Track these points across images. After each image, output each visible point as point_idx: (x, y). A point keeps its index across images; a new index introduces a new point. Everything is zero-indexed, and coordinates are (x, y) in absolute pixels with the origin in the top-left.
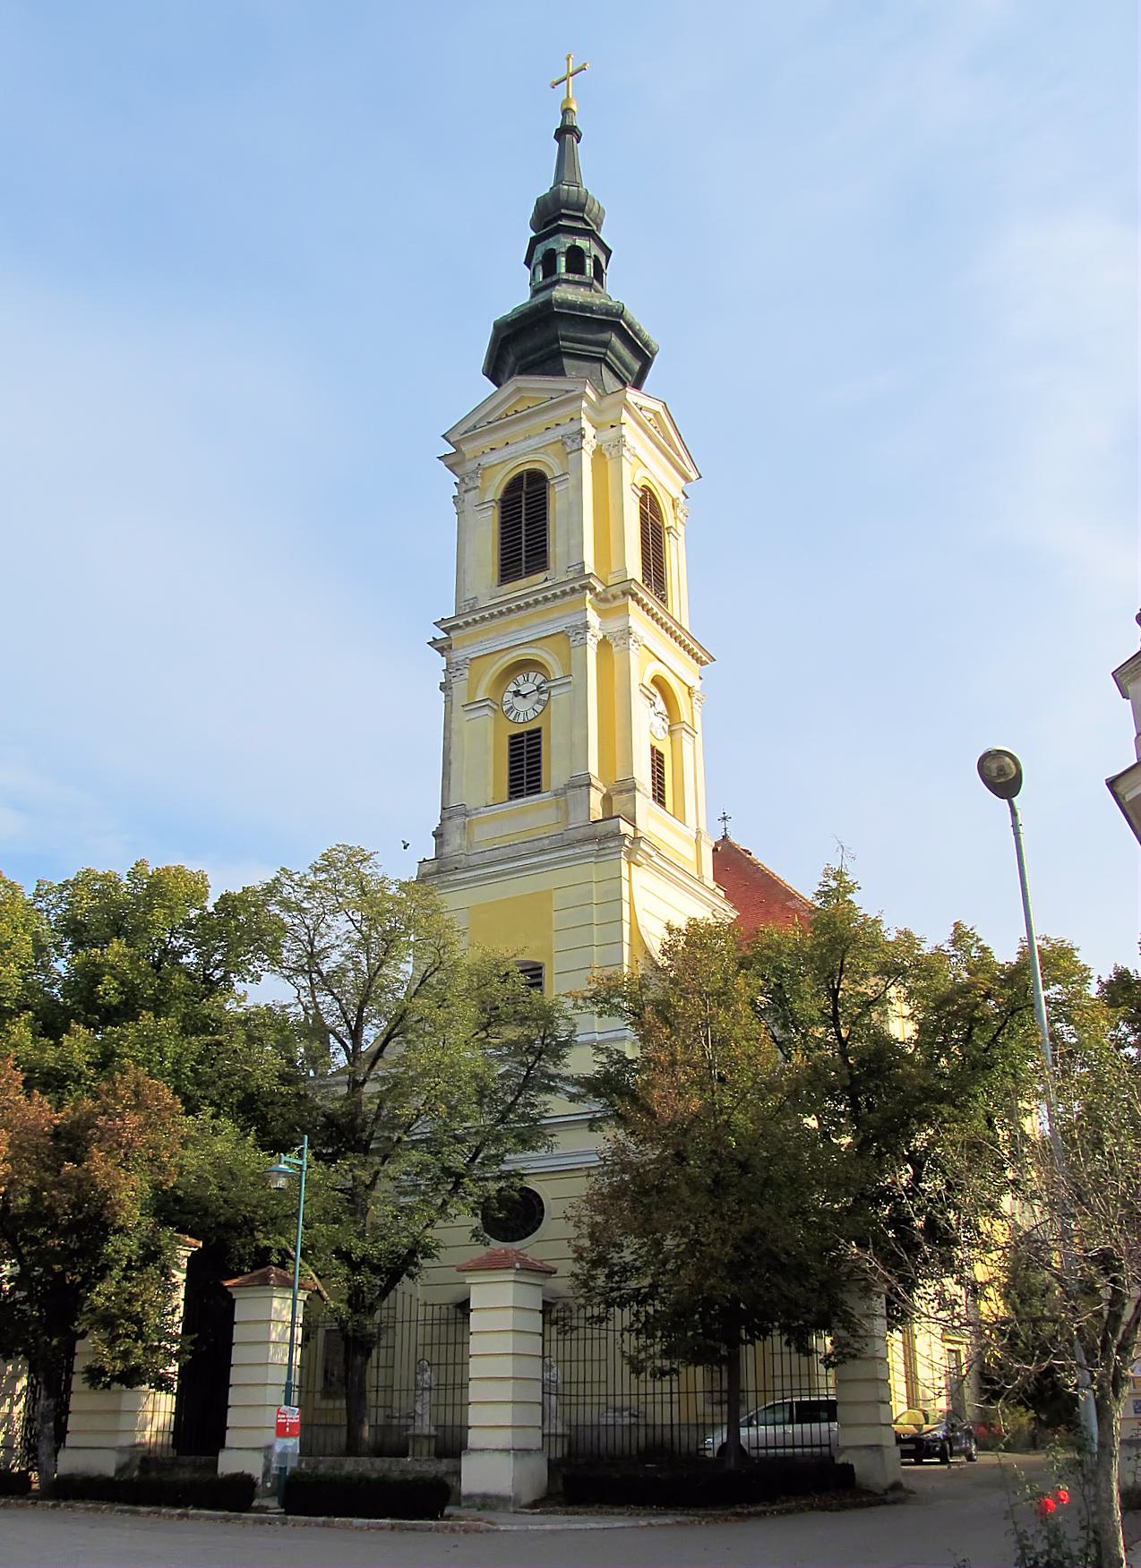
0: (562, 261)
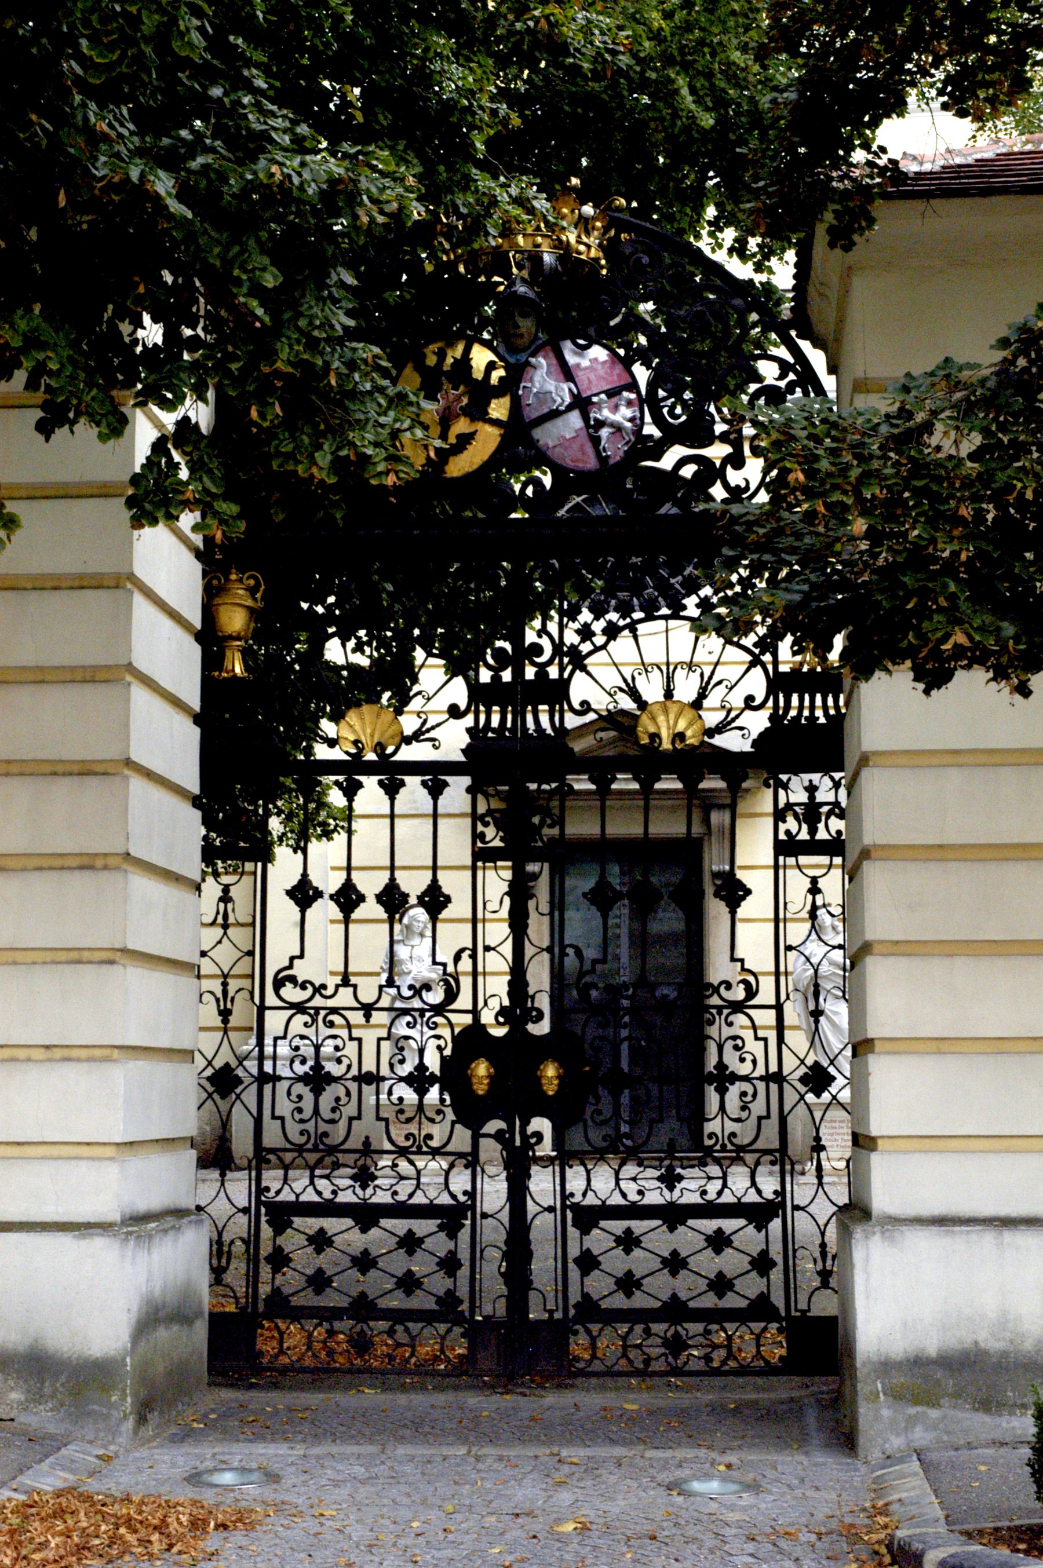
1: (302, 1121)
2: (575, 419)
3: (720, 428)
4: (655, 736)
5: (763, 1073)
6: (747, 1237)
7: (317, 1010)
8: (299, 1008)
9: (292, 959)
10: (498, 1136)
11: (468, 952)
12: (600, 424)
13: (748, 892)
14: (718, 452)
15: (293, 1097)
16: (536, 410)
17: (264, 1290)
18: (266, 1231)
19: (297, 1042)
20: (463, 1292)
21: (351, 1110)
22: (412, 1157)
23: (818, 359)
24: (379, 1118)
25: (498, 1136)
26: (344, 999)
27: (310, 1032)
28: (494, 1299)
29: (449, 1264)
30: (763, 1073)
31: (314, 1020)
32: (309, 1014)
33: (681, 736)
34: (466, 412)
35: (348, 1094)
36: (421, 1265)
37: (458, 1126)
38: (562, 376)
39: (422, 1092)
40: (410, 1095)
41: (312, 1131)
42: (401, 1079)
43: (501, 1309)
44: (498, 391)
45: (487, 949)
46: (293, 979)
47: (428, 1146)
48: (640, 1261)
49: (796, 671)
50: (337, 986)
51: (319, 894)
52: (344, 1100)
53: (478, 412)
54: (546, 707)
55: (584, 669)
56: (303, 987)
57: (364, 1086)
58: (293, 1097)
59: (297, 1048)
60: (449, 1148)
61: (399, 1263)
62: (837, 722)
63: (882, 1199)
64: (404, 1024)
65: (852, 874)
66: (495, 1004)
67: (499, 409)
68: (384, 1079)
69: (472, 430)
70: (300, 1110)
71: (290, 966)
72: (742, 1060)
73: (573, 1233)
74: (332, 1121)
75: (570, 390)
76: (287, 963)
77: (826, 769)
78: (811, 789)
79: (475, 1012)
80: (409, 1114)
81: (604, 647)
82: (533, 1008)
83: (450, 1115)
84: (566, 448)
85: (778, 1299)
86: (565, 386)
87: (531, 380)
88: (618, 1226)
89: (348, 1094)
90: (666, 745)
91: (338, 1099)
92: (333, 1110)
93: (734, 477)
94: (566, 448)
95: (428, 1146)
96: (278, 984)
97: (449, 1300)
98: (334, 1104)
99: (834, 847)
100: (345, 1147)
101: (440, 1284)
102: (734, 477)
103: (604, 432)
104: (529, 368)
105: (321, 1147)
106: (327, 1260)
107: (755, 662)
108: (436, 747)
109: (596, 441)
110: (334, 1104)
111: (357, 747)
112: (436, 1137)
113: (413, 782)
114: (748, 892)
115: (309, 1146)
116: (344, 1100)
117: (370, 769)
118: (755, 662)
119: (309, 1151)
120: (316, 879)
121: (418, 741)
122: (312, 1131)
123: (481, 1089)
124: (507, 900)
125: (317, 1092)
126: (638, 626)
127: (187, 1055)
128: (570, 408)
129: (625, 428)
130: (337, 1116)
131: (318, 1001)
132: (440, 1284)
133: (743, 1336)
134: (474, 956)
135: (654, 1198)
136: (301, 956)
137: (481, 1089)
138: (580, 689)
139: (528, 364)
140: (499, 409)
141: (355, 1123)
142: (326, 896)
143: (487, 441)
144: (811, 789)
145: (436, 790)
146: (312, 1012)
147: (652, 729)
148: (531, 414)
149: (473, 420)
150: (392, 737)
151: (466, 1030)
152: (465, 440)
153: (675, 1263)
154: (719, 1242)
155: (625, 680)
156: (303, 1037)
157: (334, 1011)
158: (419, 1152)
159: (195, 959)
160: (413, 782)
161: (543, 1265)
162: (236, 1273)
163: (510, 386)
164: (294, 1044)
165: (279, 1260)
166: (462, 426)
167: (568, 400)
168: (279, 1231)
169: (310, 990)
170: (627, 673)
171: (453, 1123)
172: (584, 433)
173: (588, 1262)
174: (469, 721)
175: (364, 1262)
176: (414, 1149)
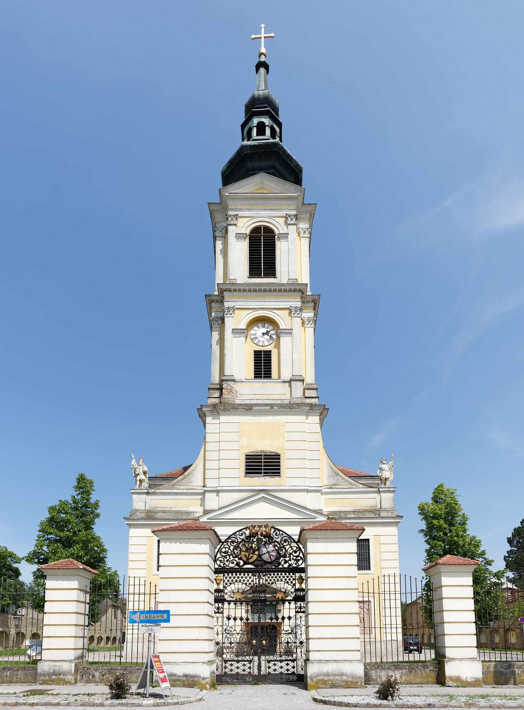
0: (268, 131)
3: (288, 556)
4: (279, 597)
6: (292, 664)
13: (368, 540)
14: (287, 559)
17: (224, 671)
18: (224, 664)
20: (252, 672)
23: (301, 546)
26: (235, 632)
28: (256, 672)
29: (250, 668)
36: (246, 668)
43: (257, 674)
44: (256, 550)
48: (276, 667)
49: (298, 588)
53: (254, 553)
61: (243, 668)
62: (304, 595)
63: (311, 658)
65: (307, 616)
73: (267, 663)
77: (302, 602)
78: (300, 604)
85: (296, 672)
88: (274, 663)
93: (290, 562)
96: (225, 630)
97: (250, 673)
99: (304, 612)
101: (248, 670)
102: (290, 562)
106: (233, 667)
107: (293, 587)
113: (232, 603)
114: (368, 540)
117: (238, 601)
118: (293, 587)
127: (212, 640)
132: (248, 670)
133: (291, 677)
135: (278, 659)
138: (226, 591)
140: (257, 553)
143: (255, 557)
144: (300, 604)
145: (290, 603)
152: (252, 557)
153: (281, 667)
154: (287, 664)
159: (213, 627)
160: (287, 602)
161: (263, 668)
162: (220, 670)
163: (258, 549)
165: (226, 667)
166: (251, 555)
168: (225, 663)
173: (269, 667)
175: (238, 668)
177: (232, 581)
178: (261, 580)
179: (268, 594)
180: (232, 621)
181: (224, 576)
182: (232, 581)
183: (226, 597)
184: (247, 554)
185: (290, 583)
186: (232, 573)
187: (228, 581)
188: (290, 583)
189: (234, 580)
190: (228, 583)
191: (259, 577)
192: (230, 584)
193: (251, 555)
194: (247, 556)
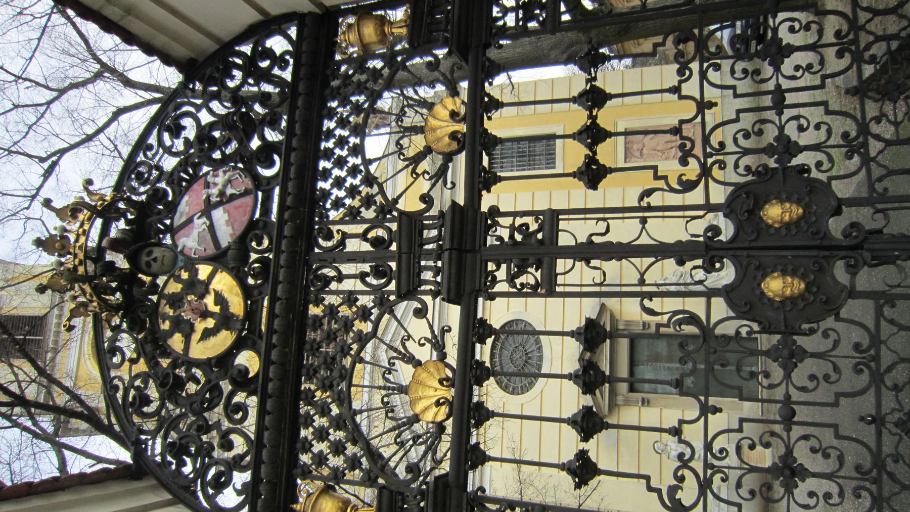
1: (841, 494)
2: (219, 215)
4: (453, 136)
5: (794, 399)
7: (707, 466)
8: (705, 486)
9: (650, 489)
10: (853, 270)
11: (646, 303)
12: (222, 194)
15: (812, 502)
16: (208, 245)
19: (744, 492)
21: (827, 437)
22: (883, 368)
24: (836, 404)
25: (853, 270)
27: (734, 475)
30: (794, 399)
31: (719, 470)
32: (712, 475)
33: (454, 115)
34: (202, 297)
35: (805, 437)
37: (843, 313)
38: (190, 225)
39: (803, 354)
40: (807, 367)
41: (855, 483)
42: (788, 376)
45: (642, 282)
46: (673, 490)
47: (868, 349)
50: (681, 441)
51: (582, 455)
52: (813, 442)
54: (425, 232)
55: (396, 201)
56: (682, 479)
57: (796, 419)
58: (812, 502)
59: (752, 493)
60: (871, 325)
64: (847, 129)
66: (700, 274)
67: (204, 271)
68: (788, 430)
69: (213, 293)
70: (828, 496)
71: (659, 491)
72: (811, 494)
74: (841, 459)
75: (198, 218)
76: (655, 495)
79: (710, 294)
80: (828, 368)
81: (380, 186)
82: (705, 235)
83: (830, 322)
84: (236, 220)
86: (196, 221)
87: (191, 249)
89: (805, 437)
90: (463, 128)
91: (813, 450)
92: (826, 456)
94: (236, 220)
95: (868, 349)
98: (819, 455)
100: (873, 445)
103: (229, 191)
104: (185, 251)
105: (874, 473)
108: (450, 330)
109: (233, 197)
110: (819, 455)
111: (443, 404)
112: (855, 338)
115: (874, 488)
116: (813, 442)
119: (880, 489)
120: (568, 455)
121: (444, 347)
122: (855, 483)
123: (796, 286)
124: (594, 263)
125: (804, 473)
126: (367, 157)
128: (210, 218)
129: (230, 177)
130: (834, 454)
131: (698, 465)
134: (651, 296)
136: (648, 478)
137: (796, 286)
138: (410, 204)
139: (182, 252)
141: (842, 432)
142: (583, 446)
143: (224, 282)
146: (709, 472)
147: (447, 139)
148: (211, 250)
149: (207, 292)
150: (438, 370)
151: (731, 304)
152: (220, 299)
155: (407, 166)
156: (739, 485)
157: (708, 447)
158: (876, 358)
164: (748, 496)
166: (209, 300)
167: (204, 219)
169: (687, 473)
170: (401, 164)
171: (838, 318)
172: (227, 206)
174: (428, 299)
176: (709, 150)
177: (354, 171)
178: (353, 246)
179: (432, 250)
180: (607, 153)
181: (306, 473)
182: (354, 171)
183: (443, 199)
184: (200, 326)
185: (367, 327)
186: (296, 421)
187: (338, 448)
188: (367, 327)
189: (352, 161)
190: (351, 449)
191: (339, 254)
192: (370, 180)
193: (209, 300)
194: (210, 323)
